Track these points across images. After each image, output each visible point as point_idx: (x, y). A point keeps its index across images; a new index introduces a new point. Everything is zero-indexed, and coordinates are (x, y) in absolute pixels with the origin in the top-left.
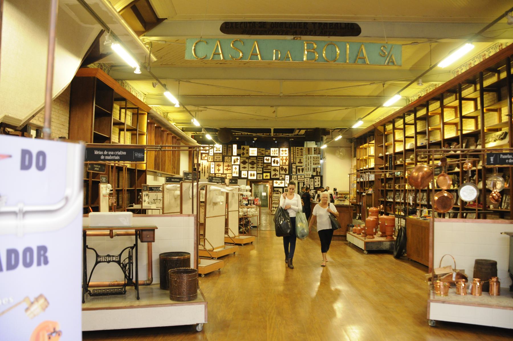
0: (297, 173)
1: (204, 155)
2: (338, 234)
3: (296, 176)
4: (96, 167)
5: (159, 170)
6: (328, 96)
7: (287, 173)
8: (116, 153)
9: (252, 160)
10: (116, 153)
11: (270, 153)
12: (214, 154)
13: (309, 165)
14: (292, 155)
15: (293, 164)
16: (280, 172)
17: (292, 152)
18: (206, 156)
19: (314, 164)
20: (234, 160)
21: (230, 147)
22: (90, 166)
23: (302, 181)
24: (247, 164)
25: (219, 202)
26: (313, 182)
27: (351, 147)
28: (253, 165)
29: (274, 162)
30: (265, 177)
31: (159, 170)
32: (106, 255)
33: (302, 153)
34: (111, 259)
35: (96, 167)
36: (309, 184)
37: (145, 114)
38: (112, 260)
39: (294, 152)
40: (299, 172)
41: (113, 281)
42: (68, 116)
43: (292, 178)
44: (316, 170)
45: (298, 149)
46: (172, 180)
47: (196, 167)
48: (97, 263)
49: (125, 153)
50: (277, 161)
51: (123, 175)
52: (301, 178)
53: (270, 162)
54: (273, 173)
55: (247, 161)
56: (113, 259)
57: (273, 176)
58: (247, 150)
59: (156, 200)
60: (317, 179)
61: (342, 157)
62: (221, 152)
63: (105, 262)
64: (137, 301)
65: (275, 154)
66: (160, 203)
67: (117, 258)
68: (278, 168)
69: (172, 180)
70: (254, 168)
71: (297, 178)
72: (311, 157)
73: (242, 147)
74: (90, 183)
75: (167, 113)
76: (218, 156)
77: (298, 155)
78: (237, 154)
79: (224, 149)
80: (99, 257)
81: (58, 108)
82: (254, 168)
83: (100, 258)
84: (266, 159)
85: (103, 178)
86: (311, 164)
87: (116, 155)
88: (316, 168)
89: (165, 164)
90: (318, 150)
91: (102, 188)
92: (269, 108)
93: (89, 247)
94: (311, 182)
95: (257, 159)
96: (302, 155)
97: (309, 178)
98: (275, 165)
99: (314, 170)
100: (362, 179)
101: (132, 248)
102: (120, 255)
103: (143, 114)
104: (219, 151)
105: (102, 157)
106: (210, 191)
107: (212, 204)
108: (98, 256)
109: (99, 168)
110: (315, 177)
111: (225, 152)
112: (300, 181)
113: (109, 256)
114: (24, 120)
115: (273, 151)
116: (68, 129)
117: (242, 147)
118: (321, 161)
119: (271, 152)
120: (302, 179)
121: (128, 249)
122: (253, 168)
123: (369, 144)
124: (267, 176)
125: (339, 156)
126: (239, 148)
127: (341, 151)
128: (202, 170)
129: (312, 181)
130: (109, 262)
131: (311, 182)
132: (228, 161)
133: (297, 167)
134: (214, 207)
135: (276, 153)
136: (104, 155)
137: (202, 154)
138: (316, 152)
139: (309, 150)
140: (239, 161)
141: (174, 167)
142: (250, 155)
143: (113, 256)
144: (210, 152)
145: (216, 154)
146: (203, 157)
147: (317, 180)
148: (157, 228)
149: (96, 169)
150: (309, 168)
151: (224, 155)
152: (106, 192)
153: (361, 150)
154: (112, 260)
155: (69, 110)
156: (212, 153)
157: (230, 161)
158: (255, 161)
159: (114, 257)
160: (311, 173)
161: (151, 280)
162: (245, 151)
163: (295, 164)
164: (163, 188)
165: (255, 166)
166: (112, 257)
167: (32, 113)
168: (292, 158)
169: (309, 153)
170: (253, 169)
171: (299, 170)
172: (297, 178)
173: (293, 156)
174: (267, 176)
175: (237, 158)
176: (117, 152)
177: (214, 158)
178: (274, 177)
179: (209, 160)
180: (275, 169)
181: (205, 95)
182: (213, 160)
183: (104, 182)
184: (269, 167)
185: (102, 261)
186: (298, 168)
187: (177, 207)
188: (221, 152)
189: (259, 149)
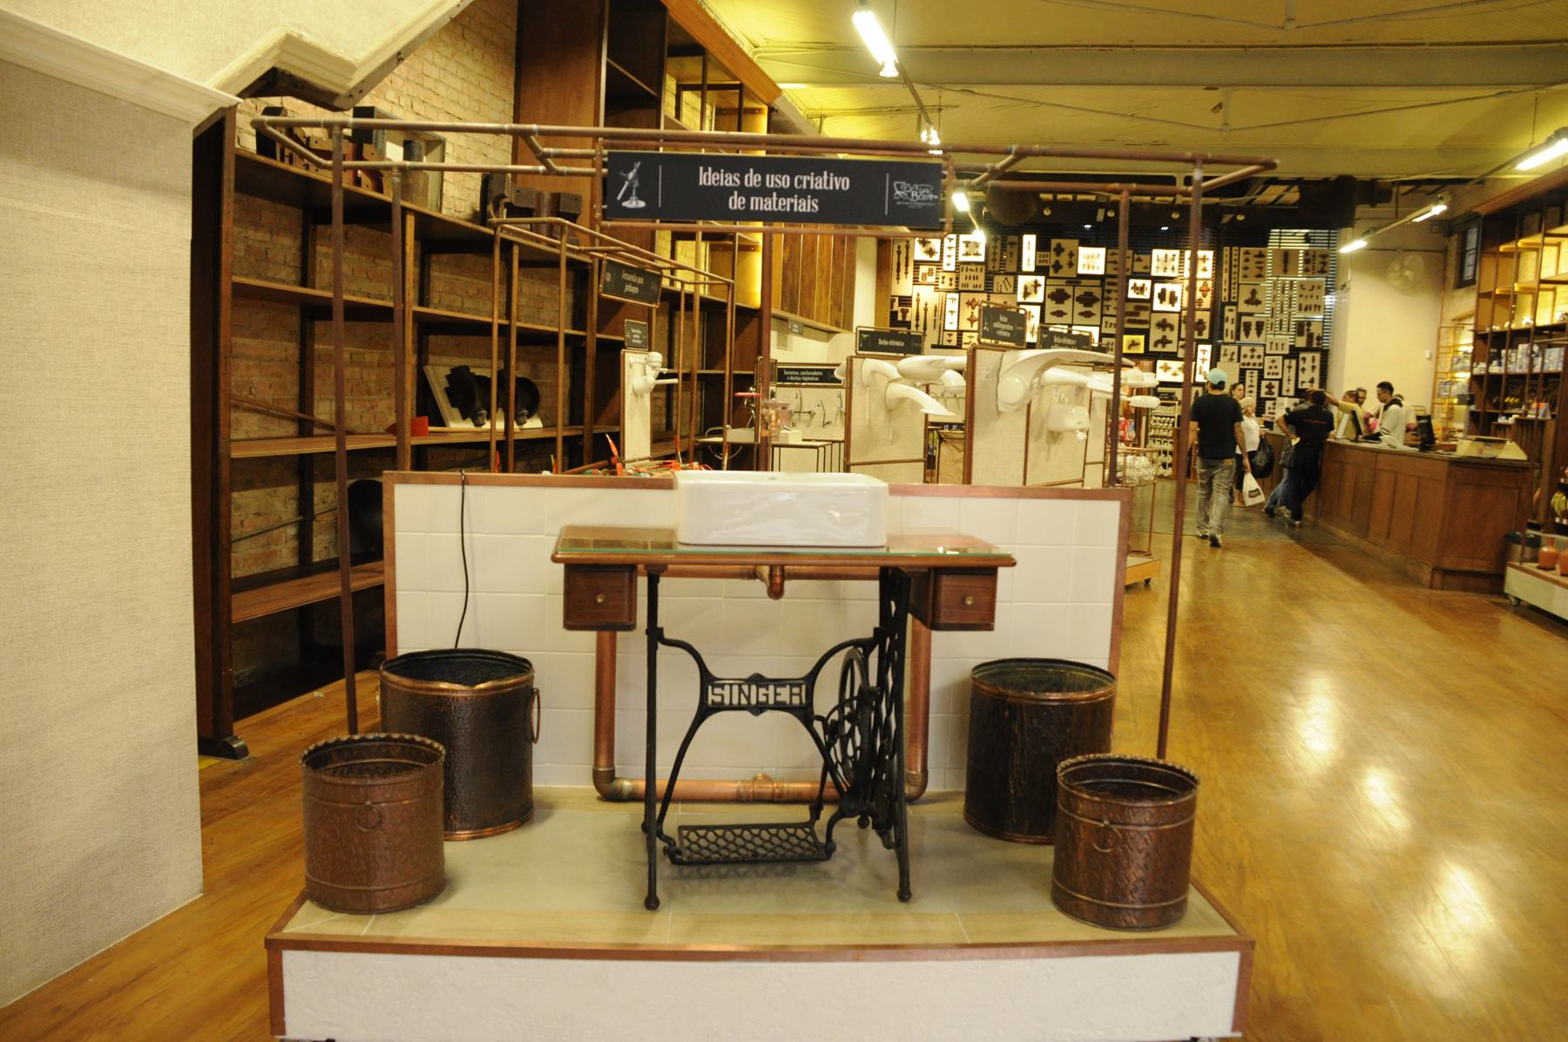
0: (1238, 338)
1: (924, 269)
2: (1466, 567)
3: (1235, 349)
4: (629, 282)
5: (795, 313)
6: (1431, 45)
7: (1206, 335)
8: (800, 182)
9: (1087, 289)
10: (800, 182)
11: (1149, 267)
12: (959, 264)
13: (1282, 311)
14: (1225, 276)
15: (1227, 308)
16: (1179, 334)
17: (1226, 266)
18: (930, 272)
19: (1300, 309)
20: (1026, 288)
21: (1012, 244)
22: (608, 277)
23: (1254, 364)
24: (1069, 302)
25: (1073, 431)
26: (1293, 370)
27: (1445, 252)
28: (1090, 306)
29: (1162, 296)
30: (1129, 348)
31: (793, 311)
32: (746, 676)
33: (1261, 268)
34: (767, 694)
35: (629, 282)
36: (1279, 377)
37: (760, 111)
38: (771, 701)
39: (1234, 263)
40: (1247, 335)
41: (748, 774)
42: (512, 102)
43: (1222, 352)
44: (1308, 330)
45: (1247, 253)
46: (881, 342)
47: (896, 307)
48: (705, 711)
49: (844, 183)
50: (1172, 294)
51: (693, 326)
52: (1252, 357)
53: (1147, 295)
54: (1156, 334)
55: (1069, 290)
56: (776, 694)
57: (1156, 345)
58: (1071, 255)
59: (796, 416)
60: (1310, 360)
61: (1411, 288)
62: (981, 259)
63: (740, 708)
64: (900, 907)
65: (1165, 269)
66: (808, 426)
67: (796, 690)
68: (1173, 320)
69: (881, 342)
70: (1093, 314)
71: (1239, 355)
72: (1292, 283)
73: (1054, 242)
74: (591, 348)
75: (822, 117)
76: (972, 274)
77: (1245, 276)
78: (1036, 267)
79: (992, 250)
80: (714, 686)
81: (478, 69)
82: (1093, 314)
83: (718, 690)
84: (1135, 288)
85: (633, 331)
86: (1290, 307)
87: (803, 194)
88: (1309, 324)
89: (811, 296)
90: (1319, 260)
91: (631, 366)
92: (1200, 92)
93: (667, 635)
94: (1286, 370)
95: (1102, 286)
96: (1259, 276)
97: (1281, 358)
98: (1166, 306)
99: (1301, 328)
100: (1500, 364)
101: (865, 645)
102: (811, 679)
103: (754, 111)
104: (977, 254)
105: (736, 202)
106: (1043, 386)
107: (1044, 436)
108: (707, 679)
109: (639, 286)
110: (1302, 355)
111: (994, 260)
112: (1249, 364)
113: (758, 680)
114: (364, 63)
115: (1162, 260)
116: (511, 151)
117: (1054, 242)
118: (1329, 300)
119: (1155, 263)
120: (1256, 360)
121: (843, 653)
122: (1088, 315)
123: (1546, 235)
124: (1134, 344)
125: (1397, 283)
126: (1042, 246)
127: (1407, 263)
128: (917, 320)
129: (1290, 367)
130: (759, 709)
131: (1286, 370)
132: (1004, 290)
133: (1240, 315)
134: (1049, 450)
135: (1169, 267)
136: (746, 192)
137: (918, 264)
138: (1310, 266)
139: (1286, 258)
140: (1041, 290)
141: (837, 305)
142: (1081, 270)
143: (779, 683)
144: (946, 260)
145: (965, 267)
146: (920, 276)
147: (1308, 365)
148: (1009, 562)
149: (629, 288)
150: (1281, 321)
151: (990, 268)
152: (646, 380)
153: (1501, 260)
154: (771, 701)
155: (513, 78)
156: (952, 261)
157: (1011, 290)
158: (1097, 292)
159: (784, 686)
160: (1286, 340)
161: (919, 780)
162: (1064, 259)
163: (1234, 308)
164: (849, 372)
165: (1096, 308)
166: (771, 687)
167: (394, 39)
168: (1225, 286)
169: (1285, 271)
170: (1087, 321)
171: (1247, 326)
172: (1239, 355)
173: (1230, 277)
174: (1134, 344)
175: (1036, 282)
176: (805, 178)
177: (957, 279)
178: (1159, 348)
179: (941, 286)
180: (1164, 320)
181: (969, 47)
182: (953, 287)
183: (636, 346)
184: (1144, 315)
185: (727, 702)
186: (1245, 319)
187: (892, 442)
188: (981, 259)
189: (1111, 251)
